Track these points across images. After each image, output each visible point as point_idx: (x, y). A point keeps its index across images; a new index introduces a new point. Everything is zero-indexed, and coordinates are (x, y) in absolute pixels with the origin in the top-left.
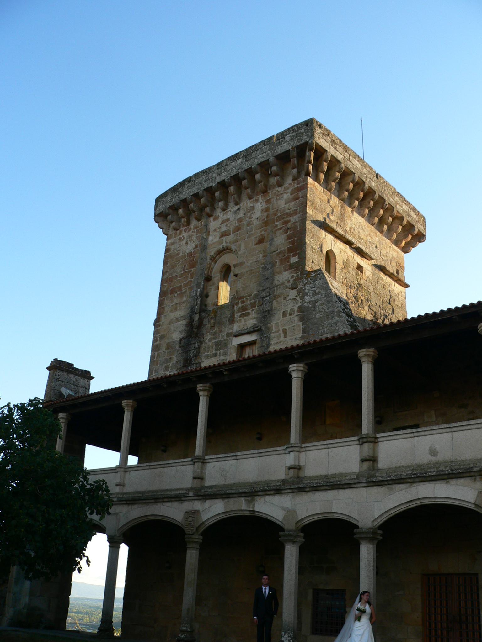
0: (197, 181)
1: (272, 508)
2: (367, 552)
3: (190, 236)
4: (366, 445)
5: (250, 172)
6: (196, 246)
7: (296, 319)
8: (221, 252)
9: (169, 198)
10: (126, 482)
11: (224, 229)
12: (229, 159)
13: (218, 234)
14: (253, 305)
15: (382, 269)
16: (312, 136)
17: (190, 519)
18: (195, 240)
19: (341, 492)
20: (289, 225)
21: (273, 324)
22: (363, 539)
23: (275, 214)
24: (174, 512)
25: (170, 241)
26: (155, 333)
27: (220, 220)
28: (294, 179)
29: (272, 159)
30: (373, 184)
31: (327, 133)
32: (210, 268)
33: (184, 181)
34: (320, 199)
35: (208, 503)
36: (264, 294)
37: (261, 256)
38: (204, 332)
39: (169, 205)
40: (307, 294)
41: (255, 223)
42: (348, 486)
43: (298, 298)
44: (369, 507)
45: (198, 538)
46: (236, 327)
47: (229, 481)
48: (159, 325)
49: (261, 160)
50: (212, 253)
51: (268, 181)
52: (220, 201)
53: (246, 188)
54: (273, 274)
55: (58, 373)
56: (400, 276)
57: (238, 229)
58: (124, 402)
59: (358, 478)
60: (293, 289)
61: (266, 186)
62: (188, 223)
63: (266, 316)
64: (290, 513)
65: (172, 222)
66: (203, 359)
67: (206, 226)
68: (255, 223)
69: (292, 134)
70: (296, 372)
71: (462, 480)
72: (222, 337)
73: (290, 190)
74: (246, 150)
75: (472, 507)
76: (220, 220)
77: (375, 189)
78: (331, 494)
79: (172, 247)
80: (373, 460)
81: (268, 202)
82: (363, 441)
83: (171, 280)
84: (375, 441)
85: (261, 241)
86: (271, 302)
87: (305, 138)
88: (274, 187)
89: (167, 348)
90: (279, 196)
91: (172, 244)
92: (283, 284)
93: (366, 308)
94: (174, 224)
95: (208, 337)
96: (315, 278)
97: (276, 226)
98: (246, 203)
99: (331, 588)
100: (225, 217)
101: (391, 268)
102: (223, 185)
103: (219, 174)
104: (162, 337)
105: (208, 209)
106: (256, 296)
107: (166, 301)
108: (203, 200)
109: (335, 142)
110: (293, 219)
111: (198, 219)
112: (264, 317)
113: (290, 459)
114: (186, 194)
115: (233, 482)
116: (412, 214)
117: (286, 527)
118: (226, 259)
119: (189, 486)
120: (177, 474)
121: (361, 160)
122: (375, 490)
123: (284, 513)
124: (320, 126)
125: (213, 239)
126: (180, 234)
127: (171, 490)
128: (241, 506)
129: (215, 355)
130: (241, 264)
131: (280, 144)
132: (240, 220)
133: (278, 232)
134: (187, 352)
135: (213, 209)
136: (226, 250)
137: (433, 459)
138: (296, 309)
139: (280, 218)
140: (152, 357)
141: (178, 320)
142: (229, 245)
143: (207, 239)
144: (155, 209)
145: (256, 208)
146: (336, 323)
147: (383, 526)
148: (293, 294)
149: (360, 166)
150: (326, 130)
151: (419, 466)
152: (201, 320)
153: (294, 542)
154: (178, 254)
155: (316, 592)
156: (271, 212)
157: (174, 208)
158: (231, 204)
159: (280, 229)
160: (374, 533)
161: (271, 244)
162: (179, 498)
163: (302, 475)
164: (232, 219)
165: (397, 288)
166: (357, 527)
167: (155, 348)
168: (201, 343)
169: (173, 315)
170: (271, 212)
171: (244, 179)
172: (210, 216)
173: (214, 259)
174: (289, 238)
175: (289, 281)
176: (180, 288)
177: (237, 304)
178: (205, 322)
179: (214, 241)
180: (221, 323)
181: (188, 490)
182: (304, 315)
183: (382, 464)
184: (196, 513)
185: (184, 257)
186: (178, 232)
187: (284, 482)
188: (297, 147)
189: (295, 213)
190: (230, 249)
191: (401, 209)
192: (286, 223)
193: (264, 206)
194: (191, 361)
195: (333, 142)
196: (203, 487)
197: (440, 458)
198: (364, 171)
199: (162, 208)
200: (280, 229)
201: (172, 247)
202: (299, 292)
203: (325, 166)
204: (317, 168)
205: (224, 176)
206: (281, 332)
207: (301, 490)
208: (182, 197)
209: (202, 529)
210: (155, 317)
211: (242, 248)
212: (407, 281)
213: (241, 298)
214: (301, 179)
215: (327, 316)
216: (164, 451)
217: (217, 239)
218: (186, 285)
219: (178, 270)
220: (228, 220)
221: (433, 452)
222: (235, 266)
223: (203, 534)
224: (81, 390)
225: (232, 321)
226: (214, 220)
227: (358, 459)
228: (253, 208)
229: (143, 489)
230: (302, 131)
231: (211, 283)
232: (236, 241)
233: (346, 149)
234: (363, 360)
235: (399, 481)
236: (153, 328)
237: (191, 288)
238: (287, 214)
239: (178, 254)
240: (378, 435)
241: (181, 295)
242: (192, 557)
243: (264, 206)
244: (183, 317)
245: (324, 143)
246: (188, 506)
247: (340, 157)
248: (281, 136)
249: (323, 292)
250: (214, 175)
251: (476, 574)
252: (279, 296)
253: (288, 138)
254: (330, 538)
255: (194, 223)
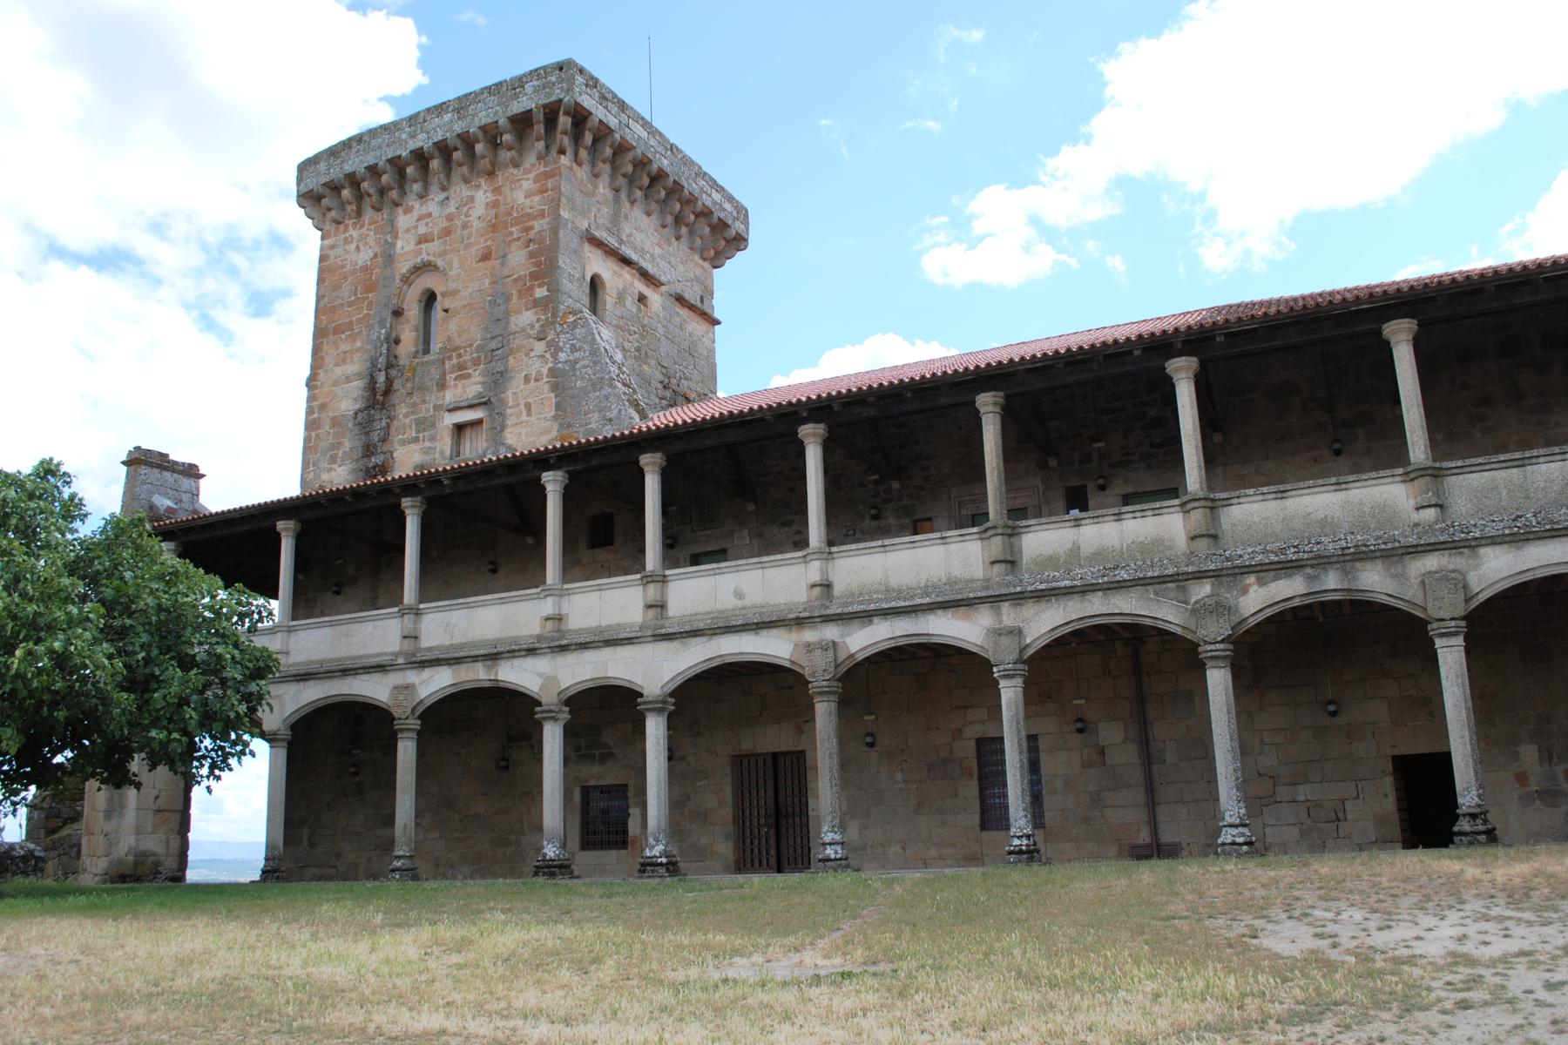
0: (373, 143)
1: (522, 675)
2: (655, 729)
3: (363, 237)
4: (651, 587)
5: (467, 141)
6: (376, 256)
7: (546, 388)
8: (418, 270)
9: (322, 166)
10: (292, 647)
11: (422, 230)
12: (428, 110)
13: (413, 240)
14: (476, 362)
15: (680, 299)
16: (569, 90)
17: (401, 697)
18: (372, 243)
19: (619, 649)
20: (532, 234)
21: (510, 393)
22: (649, 710)
23: (510, 214)
24: (375, 689)
25: (326, 242)
26: (310, 399)
27: (416, 214)
28: (540, 158)
29: (502, 122)
30: (666, 162)
31: (593, 83)
32: (401, 295)
33: (350, 139)
34: (586, 198)
35: (427, 672)
36: (493, 345)
37: (487, 282)
38: (396, 401)
39: (323, 180)
40: (561, 350)
41: (476, 225)
42: (629, 641)
43: (548, 355)
44: (655, 670)
45: (415, 724)
46: (449, 397)
47: (458, 640)
48: (315, 387)
49: (484, 121)
50: (404, 270)
51: (495, 155)
52: (416, 181)
53: (460, 165)
54: (507, 313)
55: (143, 470)
56: (706, 308)
57: (447, 232)
58: (280, 525)
59: (641, 629)
60: (540, 340)
61: (493, 164)
62: (359, 213)
63: (498, 380)
64: (550, 680)
65: (329, 210)
66: (396, 445)
67: (392, 222)
68: (476, 225)
69: (535, 83)
70: (553, 483)
71: (775, 631)
72: (426, 410)
73: (532, 175)
74: (459, 99)
75: (788, 665)
76: (416, 214)
77: (668, 170)
78: (607, 652)
79: (332, 253)
80: (660, 606)
81: (497, 191)
82: (648, 580)
83: (333, 310)
84: (664, 580)
85: (486, 257)
86: (505, 358)
87: (557, 93)
88: (507, 167)
89: (333, 426)
90: (515, 182)
91: (332, 247)
92: (523, 330)
93: (653, 362)
94: (333, 213)
95: (402, 410)
96: (574, 325)
97: (511, 234)
98: (459, 190)
99: (607, 782)
100: (424, 210)
101: (691, 295)
102: (420, 156)
103: (413, 136)
104: (323, 407)
105: (394, 194)
106: (481, 348)
107: (325, 347)
108: (385, 178)
109: (607, 97)
110: (539, 225)
111: (378, 209)
112: (495, 382)
113: (547, 607)
114: (356, 163)
115: (463, 640)
116: (728, 206)
117: (544, 701)
118: (428, 281)
119: (396, 648)
120: (374, 633)
121: (646, 125)
122: (663, 646)
123: (540, 681)
124: (582, 71)
125: (404, 245)
126: (346, 231)
127: (367, 656)
128: (478, 675)
129: (416, 440)
130: (455, 292)
131: (516, 96)
132: (450, 218)
133: (515, 245)
134: (367, 434)
135: (403, 192)
136: (425, 267)
137: (739, 603)
138: (545, 371)
139: (517, 222)
140: (307, 440)
141: (348, 379)
142: (431, 258)
143: (393, 245)
144: (298, 184)
145: (474, 201)
146: (607, 397)
147: (671, 695)
148: (540, 347)
149: (644, 134)
150: (592, 77)
151: (720, 612)
152: (389, 382)
153: (555, 719)
154: (343, 267)
155: (586, 791)
156: (502, 209)
157: (334, 187)
158: (434, 188)
159: (518, 239)
160: (664, 702)
161: (503, 264)
162: (381, 668)
163: (564, 628)
164: (435, 214)
165: (696, 326)
166: (641, 695)
167: (311, 425)
168: (391, 419)
169: (339, 371)
170: (502, 209)
171: (456, 149)
172: (397, 205)
173: (407, 280)
174: (532, 255)
175: (532, 327)
176: (349, 326)
177: (450, 358)
178: (397, 385)
179: (407, 249)
180: (423, 388)
181: (397, 655)
182: (559, 381)
183: (674, 609)
184: (409, 687)
185: (354, 272)
186: (341, 227)
187: (539, 638)
188: (545, 106)
189: (542, 215)
190: (436, 268)
191: (710, 199)
192: (528, 229)
193: (491, 197)
194: (375, 447)
195: (603, 97)
196: (419, 650)
197: (748, 602)
198: (652, 142)
199: (312, 183)
200: (518, 239)
201: (332, 253)
202: (549, 345)
203: (588, 138)
204: (577, 138)
205: (422, 141)
206: (522, 407)
207: (563, 649)
208: (348, 168)
209: (419, 711)
210: (307, 372)
211: (456, 264)
212: (717, 315)
213: (456, 349)
214: (550, 158)
215: (594, 385)
216: (338, 593)
217: (411, 247)
218: (360, 321)
219: (345, 292)
220: (429, 215)
221: (739, 595)
222: (444, 295)
223: (420, 717)
224: (185, 497)
225: (442, 386)
226: (405, 212)
227: (641, 604)
228: (471, 199)
229: (321, 656)
230: (553, 79)
231: (403, 319)
232: (444, 253)
233: (623, 106)
234: (646, 469)
235: (695, 633)
236: (304, 392)
237: (370, 327)
238: (528, 215)
239: (343, 267)
240: (668, 572)
241: (352, 338)
242: (406, 751)
243: (491, 197)
244: (359, 375)
245: (588, 102)
246: (395, 679)
247: (613, 122)
248: (519, 82)
249: (586, 347)
250: (404, 136)
251: (803, 752)
252: (518, 350)
253: (529, 88)
254: (605, 713)
255: (369, 213)
